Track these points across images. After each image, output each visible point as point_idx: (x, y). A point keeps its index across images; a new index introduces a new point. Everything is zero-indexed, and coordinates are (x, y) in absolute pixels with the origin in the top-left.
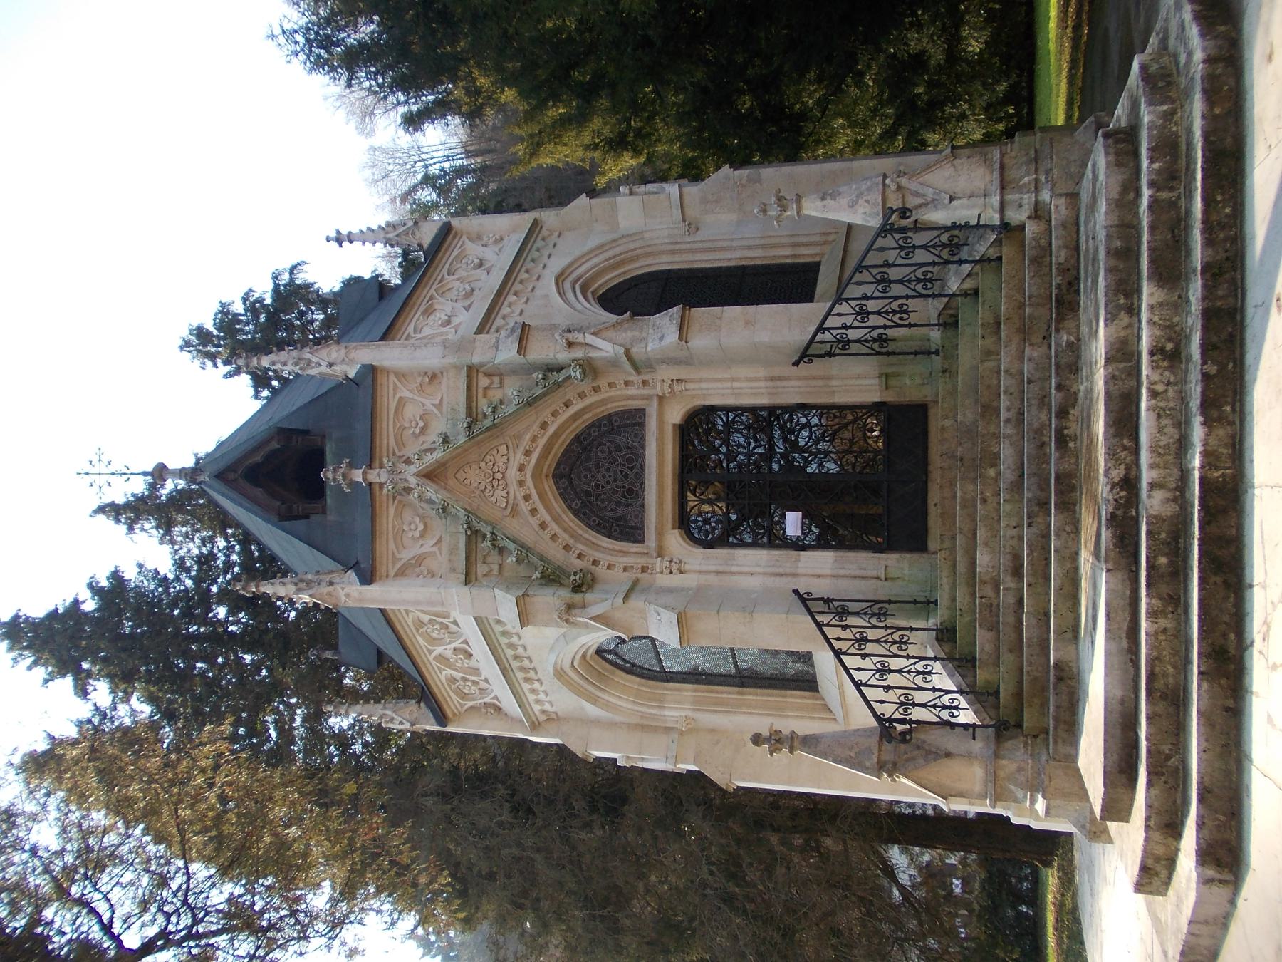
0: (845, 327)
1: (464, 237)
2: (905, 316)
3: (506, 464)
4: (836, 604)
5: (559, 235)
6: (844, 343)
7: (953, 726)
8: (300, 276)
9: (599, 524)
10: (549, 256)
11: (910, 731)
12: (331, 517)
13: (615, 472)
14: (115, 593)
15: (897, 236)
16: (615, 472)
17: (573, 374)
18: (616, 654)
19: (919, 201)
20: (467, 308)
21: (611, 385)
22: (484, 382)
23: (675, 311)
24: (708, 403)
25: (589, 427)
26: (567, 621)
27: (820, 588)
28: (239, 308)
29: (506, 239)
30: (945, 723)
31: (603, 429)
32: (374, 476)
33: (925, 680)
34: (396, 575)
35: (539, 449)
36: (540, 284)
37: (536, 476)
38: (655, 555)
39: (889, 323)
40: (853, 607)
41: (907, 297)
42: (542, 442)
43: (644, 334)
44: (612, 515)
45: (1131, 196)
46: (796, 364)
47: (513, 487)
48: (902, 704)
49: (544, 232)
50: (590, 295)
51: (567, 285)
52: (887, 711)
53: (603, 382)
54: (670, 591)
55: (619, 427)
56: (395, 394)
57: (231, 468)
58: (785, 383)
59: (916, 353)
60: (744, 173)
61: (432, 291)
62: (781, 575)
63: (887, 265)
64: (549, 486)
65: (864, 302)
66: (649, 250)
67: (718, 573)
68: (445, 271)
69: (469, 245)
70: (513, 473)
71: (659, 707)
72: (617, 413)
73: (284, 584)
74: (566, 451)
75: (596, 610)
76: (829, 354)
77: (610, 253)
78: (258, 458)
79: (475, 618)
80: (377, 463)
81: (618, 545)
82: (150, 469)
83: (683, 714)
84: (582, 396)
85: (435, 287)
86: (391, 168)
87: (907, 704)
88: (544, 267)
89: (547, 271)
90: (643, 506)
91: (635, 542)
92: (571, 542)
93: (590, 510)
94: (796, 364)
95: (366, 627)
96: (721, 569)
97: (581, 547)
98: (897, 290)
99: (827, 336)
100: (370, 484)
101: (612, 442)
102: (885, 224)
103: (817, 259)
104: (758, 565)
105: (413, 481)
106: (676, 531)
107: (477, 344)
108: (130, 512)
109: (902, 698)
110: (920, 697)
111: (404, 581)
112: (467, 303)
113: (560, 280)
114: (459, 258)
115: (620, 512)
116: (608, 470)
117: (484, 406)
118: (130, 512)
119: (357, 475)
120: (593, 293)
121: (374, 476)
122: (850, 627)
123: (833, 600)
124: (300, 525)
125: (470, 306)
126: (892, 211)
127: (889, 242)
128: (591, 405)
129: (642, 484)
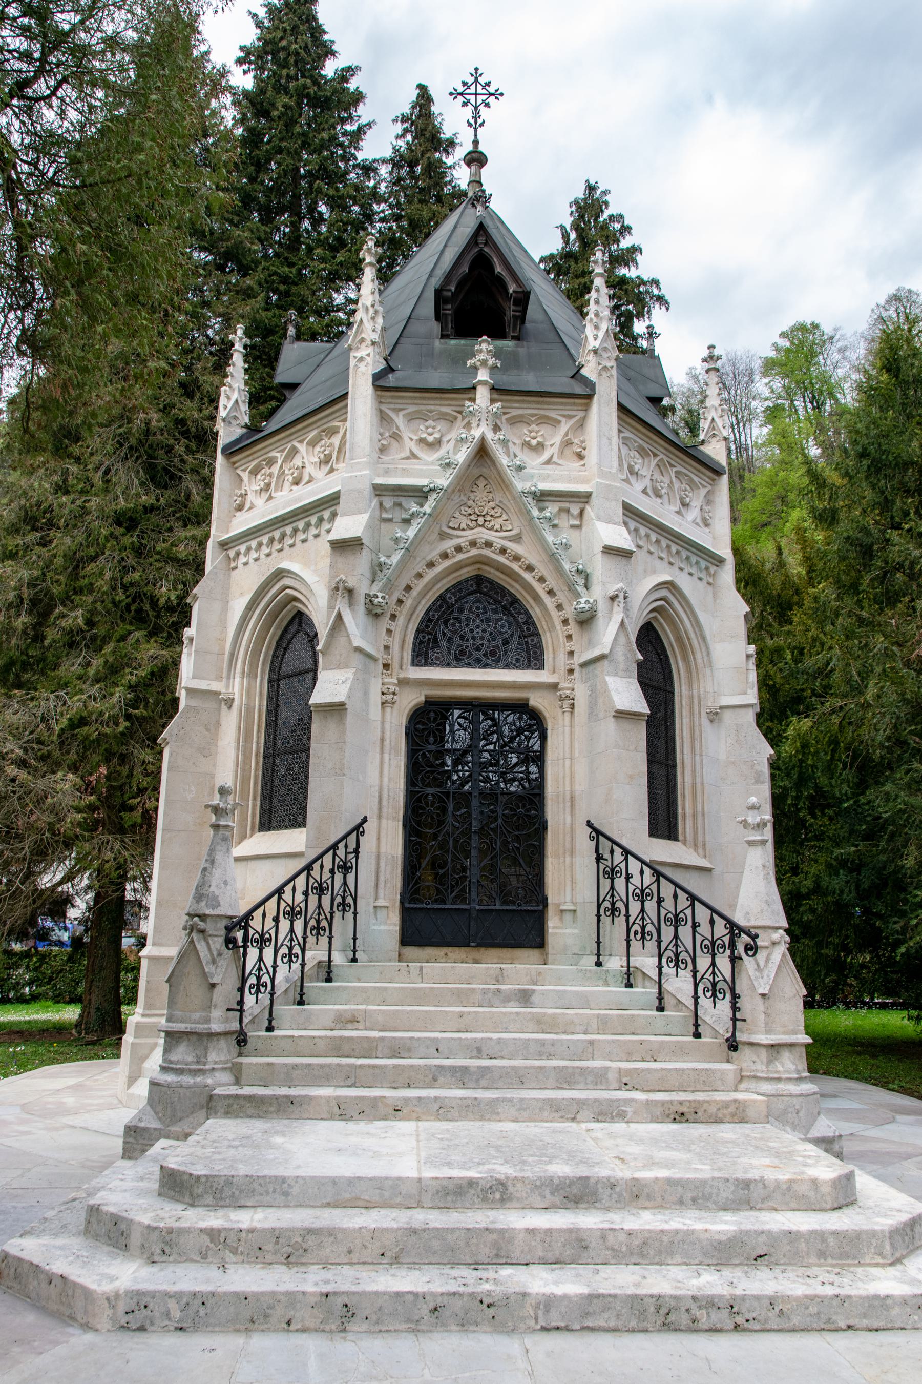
0: (628, 877)
1: (709, 487)
2: (639, 936)
3: (492, 529)
4: (354, 861)
5: (709, 584)
6: (612, 874)
7: (241, 990)
8: (657, 306)
9: (430, 620)
10: (691, 574)
11: (236, 946)
12: (438, 343)
13: (482, 638)
14: (339, 99)
15: (726, 940)
16: (482, 638)
17: (583, 600)
18: (298, 632)
19: (762, 964)
20: (644, 491)
21: (569, 637)
22: (575, 510)
23: (643, 707)
24: (549, 732)
25: (527, 613)
26: (337, 589)
27: (368, 843)
28: (626, 243)
29: (707, 530)
30: (244, 980)
31: (525, 627)
32: (483, 395)
33: (283, 956)
34: (381, 411)
35: (507, 562)
36: (665, 564)
37: (480, 561)
38: (402, 676)
39: (631, 920)
40: (351, 878)
41: (659, 942)
42: (515, 566)
43: (620, 673)
44: (440, 634)
45: (793, 1205)
46: (589, 824)
47: (470, 535)
48: (262, 936)
49: (713, 569)
50: (654, 614)
51: (664, 593)
52: (256, 923)
53: (573, 628)
54: (366, 693)
55: (527, 642)
56: (564, 416)
57: (489, 241)
58: (568, 810)
59: (598, 943)
60: (766, 770)
61: (661, 456)
62: (380, 802)
63: (695, 926)
64: (466, 573)
65: (655, 898)
66: (694, 674)
67: (382, 740)
68: (679, 468)
69: (703, 492)
70: (484, 534)
71: (243, 673)
72: (540, 641)
73: (373, 293)
74: (503, 589)
75: (348, 617)
76: (599, 858)
77: (692, 635)
78: (498, 269)
79: (338, 492)
80: (496, 396)
81: (410, 639)
82: (481, 148)
83: (236, 697)
84: (559, 607)
85: (665, 459)
86: (733, 392)
87: (262, 941)
88: (681, 569)
89: (677, 572)
90: (448, 665)
91: (413, 656)
92: (414, 593)
93: (444, 612)
94: (589, 824)
95: (324, 373)
96: (387, 743)
97: (409, 603)
98: (635, 907)
99: (618, 857)
100: (474, 388)
101: (512, 635)
102: (741, 930)
103: (681, 837)
104: (390, 779)
105: (477, 433)
106: (423, 699)
107: (614, 503)
108: (421, 120)
109: (267, 936)
110: (268, 953)
111: (376, 420)
112: (649, 491)
113: (670, 585)
114: (691, 483)
115: (443, 643)
116: (484, 631)
117: (552, 509)
118: (421, 120)
119: (483, 375)
120: (655, 618)
121: (483, 395)
122: (333, 877)
123: (357, 857)
124: (428, 308)
125: (697, 524)
126: (754, 937)
127: (721, 929)
128: (550, 615)
129: (469, 665)
